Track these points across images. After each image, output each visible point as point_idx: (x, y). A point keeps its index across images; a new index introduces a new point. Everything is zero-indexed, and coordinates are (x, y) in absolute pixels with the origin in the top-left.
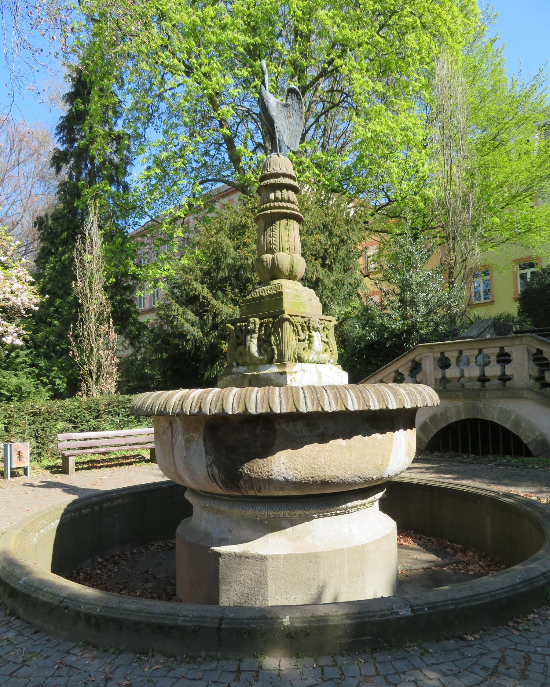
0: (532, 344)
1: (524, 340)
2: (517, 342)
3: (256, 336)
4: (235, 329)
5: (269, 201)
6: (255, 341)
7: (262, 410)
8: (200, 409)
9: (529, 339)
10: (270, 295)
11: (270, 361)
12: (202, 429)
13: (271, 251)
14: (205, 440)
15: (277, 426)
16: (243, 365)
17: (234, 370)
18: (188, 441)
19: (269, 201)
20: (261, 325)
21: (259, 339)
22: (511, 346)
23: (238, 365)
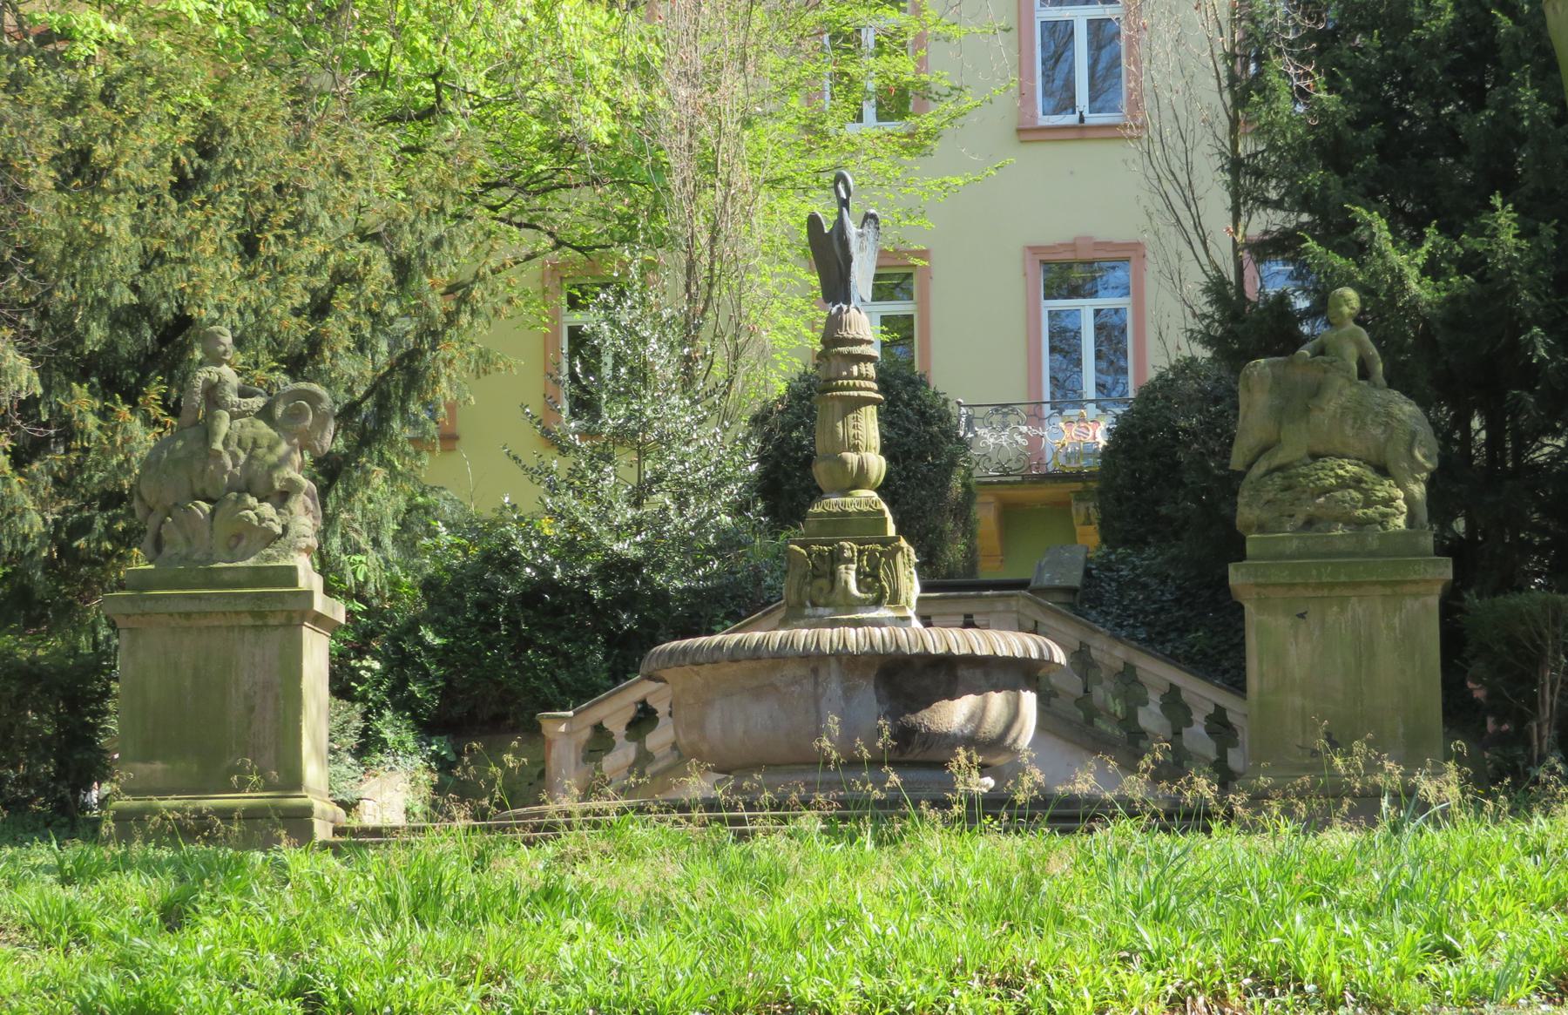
0: (1028, 612)
1: (1013, 602)
2: (1000, 606)
3: (854, 567)
4: (810, 555)
5: (850, 376)
6: (853, 573)
7: (941, 650)
8: (898, 646)
9: (1022, 602)
10: (860, 513)
11: (877, 603)
12: (873, 674)
13: (856, 448)
14: (876, 687)
15: (960, 673)
16: (826, 606)
17: (808, 611)
18: (848, 693)
19: (850, 376)
20: (860, 552)
21: (858, 572)
22: (987, 613)
23: (814, 605)
